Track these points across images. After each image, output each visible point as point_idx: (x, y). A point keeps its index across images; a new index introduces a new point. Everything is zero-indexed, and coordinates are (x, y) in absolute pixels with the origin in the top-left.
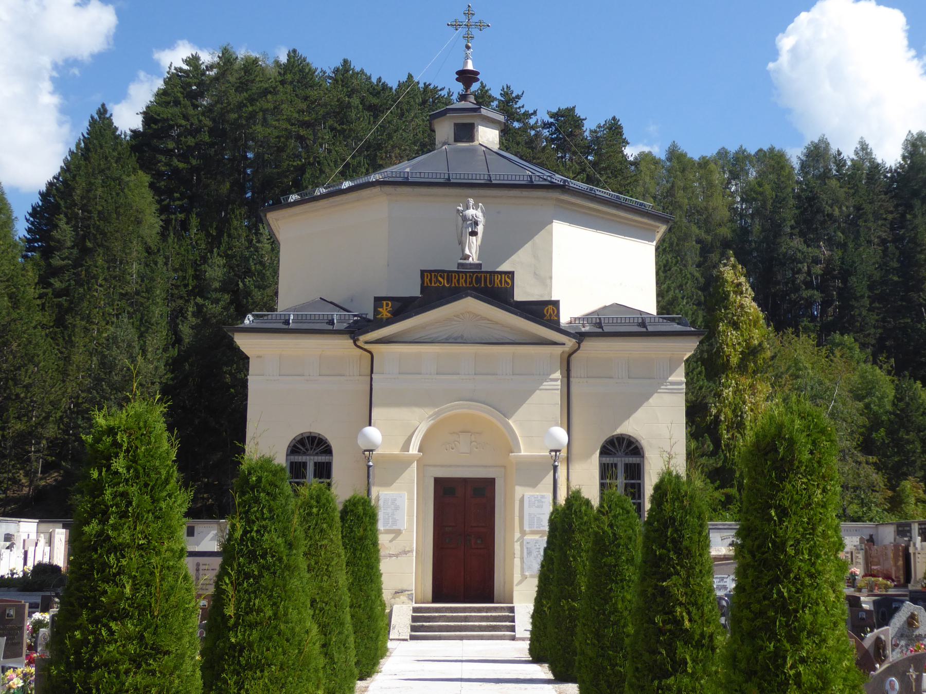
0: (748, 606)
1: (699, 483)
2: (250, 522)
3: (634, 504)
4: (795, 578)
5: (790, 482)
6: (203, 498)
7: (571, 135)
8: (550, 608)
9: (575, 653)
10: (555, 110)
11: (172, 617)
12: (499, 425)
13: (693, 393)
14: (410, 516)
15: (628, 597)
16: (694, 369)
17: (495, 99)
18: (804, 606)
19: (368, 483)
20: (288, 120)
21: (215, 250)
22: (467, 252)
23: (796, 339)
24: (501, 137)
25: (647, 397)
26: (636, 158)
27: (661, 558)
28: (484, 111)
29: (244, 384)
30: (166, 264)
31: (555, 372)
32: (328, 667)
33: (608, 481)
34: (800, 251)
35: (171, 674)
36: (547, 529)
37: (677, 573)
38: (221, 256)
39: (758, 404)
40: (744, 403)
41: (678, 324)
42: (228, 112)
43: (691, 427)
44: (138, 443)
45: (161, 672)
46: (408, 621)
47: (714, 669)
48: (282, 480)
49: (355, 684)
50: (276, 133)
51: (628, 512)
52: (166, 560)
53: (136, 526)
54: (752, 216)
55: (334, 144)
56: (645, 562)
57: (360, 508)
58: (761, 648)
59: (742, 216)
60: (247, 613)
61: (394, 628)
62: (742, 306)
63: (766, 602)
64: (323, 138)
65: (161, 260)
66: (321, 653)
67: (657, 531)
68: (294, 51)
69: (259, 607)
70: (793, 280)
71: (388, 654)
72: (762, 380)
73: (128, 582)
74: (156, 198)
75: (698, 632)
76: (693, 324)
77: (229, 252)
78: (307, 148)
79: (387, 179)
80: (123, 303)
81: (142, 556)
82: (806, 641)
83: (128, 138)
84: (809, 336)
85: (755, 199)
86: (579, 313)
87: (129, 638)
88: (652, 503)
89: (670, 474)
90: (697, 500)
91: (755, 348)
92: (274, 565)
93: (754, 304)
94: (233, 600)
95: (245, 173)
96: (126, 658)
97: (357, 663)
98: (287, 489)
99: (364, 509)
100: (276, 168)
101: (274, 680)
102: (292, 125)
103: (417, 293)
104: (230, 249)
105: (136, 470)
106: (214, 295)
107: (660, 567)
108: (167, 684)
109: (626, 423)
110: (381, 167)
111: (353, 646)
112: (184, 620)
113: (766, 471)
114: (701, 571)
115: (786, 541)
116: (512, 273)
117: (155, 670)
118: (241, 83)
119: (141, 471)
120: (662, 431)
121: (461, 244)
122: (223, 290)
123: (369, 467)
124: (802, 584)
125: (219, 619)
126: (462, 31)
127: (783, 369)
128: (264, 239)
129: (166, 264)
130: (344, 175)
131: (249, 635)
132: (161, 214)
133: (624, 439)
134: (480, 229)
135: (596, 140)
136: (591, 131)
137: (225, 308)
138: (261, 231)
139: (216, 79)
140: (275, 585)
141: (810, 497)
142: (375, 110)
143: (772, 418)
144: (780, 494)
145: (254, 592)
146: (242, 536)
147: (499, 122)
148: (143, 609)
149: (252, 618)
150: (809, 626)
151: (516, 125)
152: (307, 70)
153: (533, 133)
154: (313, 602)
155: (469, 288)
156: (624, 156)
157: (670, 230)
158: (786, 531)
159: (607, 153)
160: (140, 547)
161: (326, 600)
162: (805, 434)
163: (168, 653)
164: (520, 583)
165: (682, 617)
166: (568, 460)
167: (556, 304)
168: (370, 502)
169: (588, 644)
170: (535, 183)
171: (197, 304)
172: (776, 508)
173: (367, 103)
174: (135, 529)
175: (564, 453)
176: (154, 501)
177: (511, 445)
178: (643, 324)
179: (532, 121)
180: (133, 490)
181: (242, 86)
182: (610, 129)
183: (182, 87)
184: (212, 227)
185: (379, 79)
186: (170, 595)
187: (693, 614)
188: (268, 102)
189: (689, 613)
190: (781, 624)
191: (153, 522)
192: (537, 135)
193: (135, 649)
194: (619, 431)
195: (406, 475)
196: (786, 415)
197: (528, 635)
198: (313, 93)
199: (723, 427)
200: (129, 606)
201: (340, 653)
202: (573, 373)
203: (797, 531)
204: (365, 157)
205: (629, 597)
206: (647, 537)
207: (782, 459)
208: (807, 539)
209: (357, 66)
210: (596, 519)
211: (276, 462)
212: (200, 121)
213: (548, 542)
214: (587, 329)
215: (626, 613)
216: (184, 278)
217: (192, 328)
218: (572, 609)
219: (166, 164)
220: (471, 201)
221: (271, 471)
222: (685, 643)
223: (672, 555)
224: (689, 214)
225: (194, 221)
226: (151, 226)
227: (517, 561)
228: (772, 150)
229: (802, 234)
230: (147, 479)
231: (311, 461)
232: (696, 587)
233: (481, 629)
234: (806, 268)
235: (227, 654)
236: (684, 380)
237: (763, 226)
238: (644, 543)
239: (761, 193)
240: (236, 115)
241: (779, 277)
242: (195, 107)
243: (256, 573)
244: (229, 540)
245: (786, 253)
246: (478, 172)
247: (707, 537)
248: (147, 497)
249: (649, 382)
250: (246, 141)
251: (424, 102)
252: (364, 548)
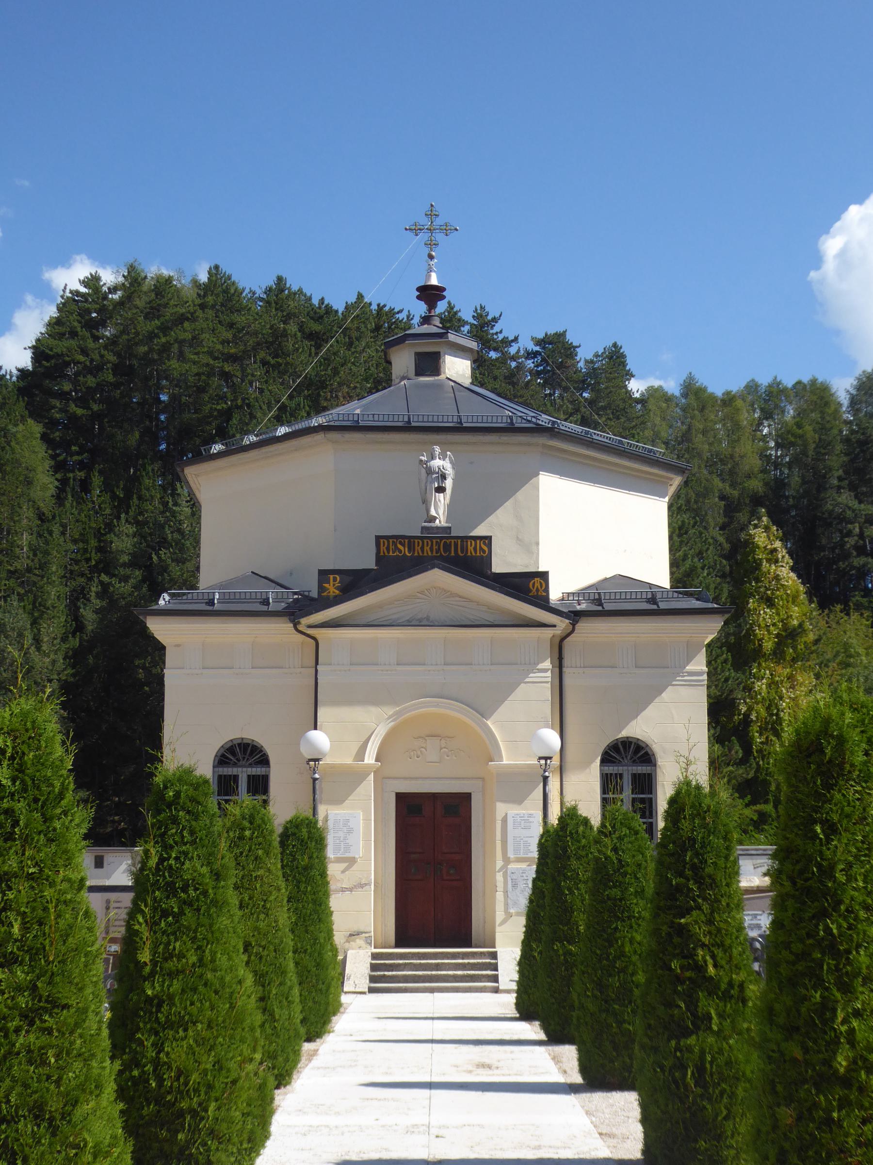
0: (787, 946)
1: (724, 795)
2: (167, 848)
3: (644, 823)
4: (847, 910)
5: (840, 791)
6: (113, 822)
7: (561, 366)
8: (540, 953)
9: (572, 1008)
10: (541, 336)
11: (71, 962)
12: (477, 728)
13: (716, 686)
14: (367, 841)
15: (637, 938)
16: (718, 656)
17: (466, 323)
18: (859, 946)
19: (314, 800)
20: (210, 353)
21: (123, 516)
22: (433, 512)
23: (846, 618)
24: (473, 369)
26: (642, 394)
27: (678, 889)
28: (452, 337)
29: (160, 681)
30: (63, 533)
32: (267, 1026)
33: (611, 795)
34: (849, 508)
35: (72, 1033)
36: (536, 855)
37: (699, 908)
38: (130, 523)
39: (799, 697)
40: (781, 698)
41: (697, 599)
42: (137, 344)
43: (715, 728)
44: (25, 748)
45: (59, 1031)
46: (365, 970)
47: (745, 1025)
48: (206, 795)
49: (301, 1047)
50: (195, 369)
51: (636, 833)
52: (62, 892)
53: (24, 851)
54: (790, 465)
55: (266, 382)
56: (657, 894)
57: (304, 830)
58: (805, 998)
59: (777, 465)
60: (166, 960)
61: (349, 979)
62: (777, 578)
63: (811, 941)
64: (253, 375)
65: (56, 529)
66: (258, 1008)
67: (672, 855)
68: (217, 267)
69: (180, 951)
70: (842, 544)
71: (342, 1010)
72: (804, 669)
73: (16, 920)
74: (50, 452)
75: (726, 980)
76: (716, 600)
77: (140, 518)
78: (233, 387)
79: (332, 424)
80: (12, 583)
81: (32, 888)
82: (861, 989)
83: (14, 379)
84: (862, 615)
85: (792, 444)
86: (574, 586)
87: (19, 989)
88: (666, 820)
89: (688, 783)
90: (723, 817)
91: (794, 630)
92: (198, 900)
93: (792, 575)
94: (148, 943)
95: (158, 419)
96: (16, 1013)
97: (304, 1021)
98: (212, 803)
99: (309, 832)
100: (195, 413)
101: (200, 1041)
102: (215, 359)
103: (370, 563)
104: (141, 513)
105: (23, 782)
106: (122, 571)
107: (676, 900)
108: (66, 1044)
109: (634, 723)
110: (325, 409)
111: (297, 1000)
112: (86, 966)
113: (809, 777)
114: (728, 905)
115: (835, 864)
116: (489, 538)
117: (51, 1028)
118: (152, 308)
119: (30, 783)
120: (678, 733)
121: (426, 502)
122: (133, 564)
123: (315, 780)
124: (856, 918)
125: (132, 966)
126: (423, 236)
127: (829, 656)
128: (182, 501)
129: (63, 533)
130: (279, 420)
131: (169, 986)
132: (56, 472)
133: (631, 743)
134: (449, 484)
135: (593, 372)
136: (586, 361)
137: (136, 587)
138: (179, 491)
139: (121, 303)
140: (199, 925)
141: (864, 809)
142: (317, 339)
143: (816, 710)
144: (827, 806)
145: (174, 933)
146: (158, 864)
147: (471, 350)
148: (36, 953)
149: (171, 965)
150: (864, 971)
151: (493, 355)
152: (232, 291)
153: (514, 364)
154: (247, 947)
155: (436, 558)
156: (629, 393)
157: (686, 483)
158: (835, 852)
159: (606, 388)
160: (30, 877)
161: (263, 943)
162: (858, 730)
163: (66, 1007)
164: (503, 922)
165: (705, 962)
166: (561, 769)
167: (544, 576)
168: (316, 822)
169: (588, 996)
170: (517, 425)
171: (101, 583)
172: (823, 823)
173: (307, 331)
174: (23, 854)
175: (556, 761)
176: (46, 819)
177: (490, 753)
178: (653, 600)
179: (513, 350)
180: (20, 806)
181: (153, 312)
182: (611, 358)
183: (79, 315)
184: (118, 487)
185: (322, 301)
186: (68, 935)
187: (718, 959)
188: (185, 331)
189: (713, 957)
190: (829, 968)
191: (46, 846)
192: (519, 367)
193: (27, 1003)
195: (361, 790)
196: (834, 706)
197: (514, 986)
198: (240, 319)
199: (755, 728)
200: (18, 949)
201: (281, 1008)
202: (566, 662)
203: (850, 852)
204: (306, 397)
205: (638, 938)
206: (660, 863)
207: (830, 761)
208: (862, 862)
209: (294, 284)
210: (597, 842)
211: (198, 773)
212: (102, 356)
213: (537, 872)
214: (583, 606)
215: (635, 958)
216: (85, 551)
217: (96, 612)
218: (570, 953)
219: (61, 410)
220: (437, 449)
221: (192, 785)
222: (709, 994)
223: (692, 885)
224: (710, 465)
225: (97, 480)
226: (44, 488)
227: (500, 896)
228: (814, 382)
229: (852, 487)
230: (37, 792)
231: (243, 773)
232: (722, 925)
233: (456, 979)
234: (857, 530)
235: (142, 1009)
236: (705, 669)
237: (803, 477)
238: (657, 870)
239: (801, 437)
240: (146, 348)
241: (824, 542)
242: (96, 338)
243: (176, 910)
244: (142, 869)
245: (833, 511)
246: (446, 413)
247: (736, 862)
248: (37, 815)
249: (662, 672)
250: (158, 380)
251: (378, 328)
252: (309, 880)
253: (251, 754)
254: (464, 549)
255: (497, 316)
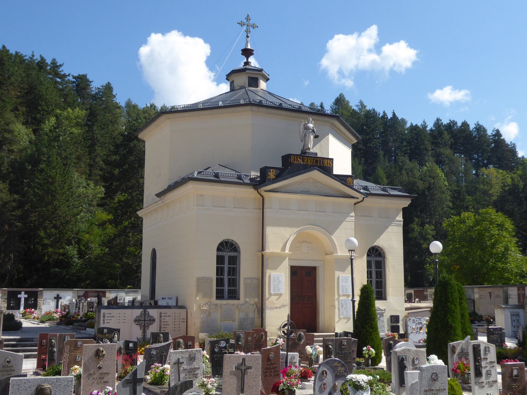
25: (387, 227)
31: (352, 212)
151: (58, 80)
194: (375, 244)
227: (337, 310)
253: (227, 245)
254: (323, 163)
255: (62, 64)
